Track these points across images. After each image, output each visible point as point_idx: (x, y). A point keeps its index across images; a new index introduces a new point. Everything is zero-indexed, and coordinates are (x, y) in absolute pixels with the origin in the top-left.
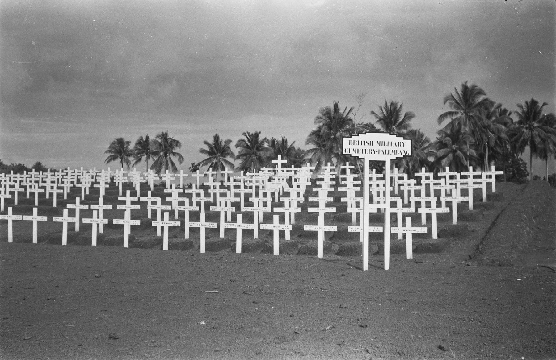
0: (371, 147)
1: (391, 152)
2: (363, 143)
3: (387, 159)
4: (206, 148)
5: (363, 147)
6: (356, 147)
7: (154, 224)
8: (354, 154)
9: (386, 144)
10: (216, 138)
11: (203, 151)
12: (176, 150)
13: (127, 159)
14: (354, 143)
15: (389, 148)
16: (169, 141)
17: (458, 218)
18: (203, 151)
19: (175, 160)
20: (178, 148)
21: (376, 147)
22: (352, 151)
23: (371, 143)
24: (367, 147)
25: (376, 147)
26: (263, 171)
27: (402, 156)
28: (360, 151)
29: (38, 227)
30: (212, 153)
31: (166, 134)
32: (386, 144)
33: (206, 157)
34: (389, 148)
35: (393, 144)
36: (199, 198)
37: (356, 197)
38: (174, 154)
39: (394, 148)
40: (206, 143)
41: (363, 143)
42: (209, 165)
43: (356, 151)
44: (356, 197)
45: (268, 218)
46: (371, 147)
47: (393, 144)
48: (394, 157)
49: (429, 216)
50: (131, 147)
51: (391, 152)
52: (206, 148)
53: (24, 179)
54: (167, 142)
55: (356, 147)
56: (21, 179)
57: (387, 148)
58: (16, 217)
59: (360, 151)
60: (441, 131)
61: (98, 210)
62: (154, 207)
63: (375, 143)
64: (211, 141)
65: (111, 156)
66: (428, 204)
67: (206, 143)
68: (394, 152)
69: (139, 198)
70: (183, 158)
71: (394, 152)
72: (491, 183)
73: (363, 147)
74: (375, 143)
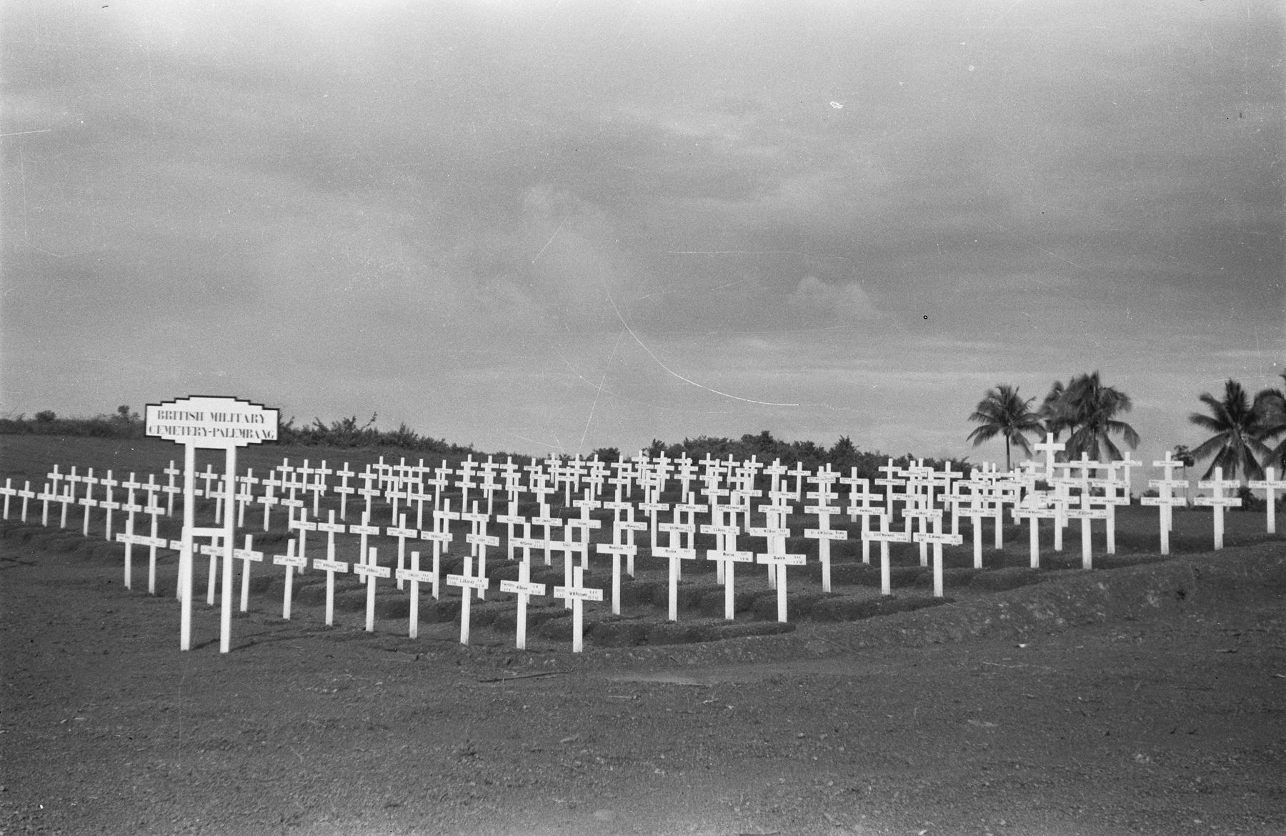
0: (199, 424)
1: (237, 433)
3: (230, 446)
4: (1208, 412)
5: (184, 423)
6: (170, 423)
8: (166, 436)
9: (228, 418)
10: (1233, 388)
11: (1199, 419)
12: (1118, 417)
13: (1019, 435)
14: (167, 416)
15: (235, 425)
16: (1102, 394)
17: (419, 620)
18: (1199, 419)
19: (1116, 438)
20: (1123, 411)
21: (208, 423)
22: (163, 430)
23: (198, 416)
24: (192, 423)
25: (208, 423)
26: (1023, 471)
27: (259, 441)
28: (179, 431)
29: (180, 617)
30: (1220, 424)
31: (1095, 377)
32: (228, 418)
33: (1207, 434)
34: (235, 425)
35: (242, 418)
36: (519, 540)
37: (788, 552)
39: (243, 425)
40: (1206, 399)
42: (1215, 453)
43: (171, 430)
44: (788, 552)
46: (199, 424)
47: (242, 418)
48: (243, 442)
50: (1034, 407)
51: (237, 433)
52: (1208, 412)
53: (946, 484)
54: (1097, 397)
55: (170, 423)
56: (937, 483)
57: (231, 426)
63: (207, 416)
64: (1220, 396)
65: (982, 428)
67: (1206, 399)
68: (244, 433)
69: (419, 533)
70: (1136, 435)
71: (244, 433)
72: (1103, 522)
73: (184, 423)
74: (207, 416)
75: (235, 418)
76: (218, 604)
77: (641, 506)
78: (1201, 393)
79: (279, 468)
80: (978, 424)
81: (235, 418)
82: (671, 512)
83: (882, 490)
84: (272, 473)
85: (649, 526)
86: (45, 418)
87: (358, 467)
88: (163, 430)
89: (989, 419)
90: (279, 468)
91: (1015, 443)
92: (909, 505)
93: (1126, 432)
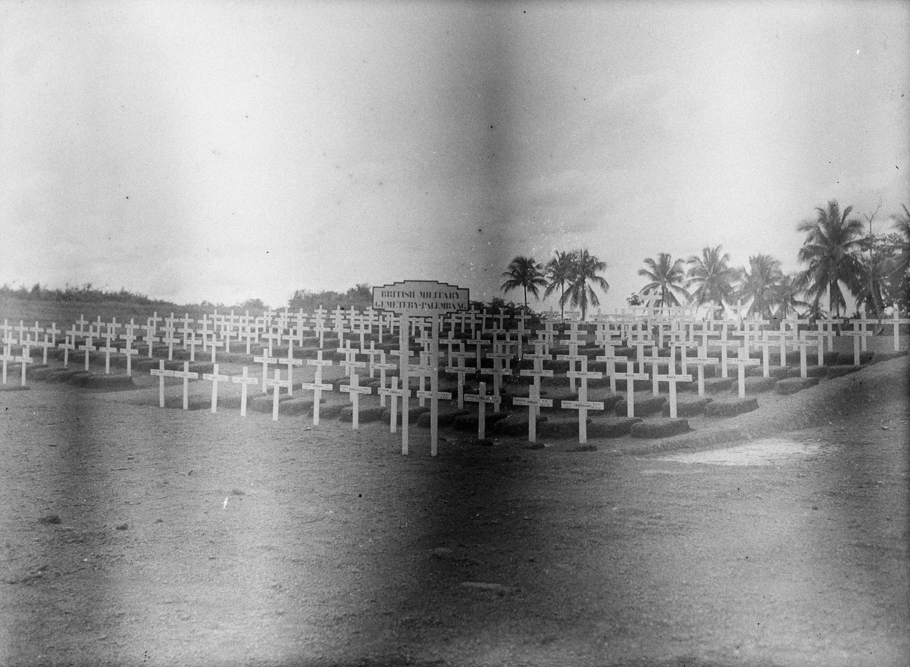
1: (439, 306)
2: (401, 295)
5: (401, 299)
6: (391, 299)
7: (87, 322)
11: (642, 272)
12: (598, 273)
18: (642, 272)
22: (385, 304)
33: (647, 281)
38: (595, 278)
40: (648, 261)
41: (401, 295)
45: (286, 332)
49: (225, 337)
51: (439, 306)
55: (391, 299)
58: (488, 316)
59: (397, 305)
60: (522, 259)
61: (499, 319)
62: (219, 323)
65: (511, 281)
66: (664, 370)
67: (648, 261)
75: (438, 295)
76: (399, 433)
77: (15, 342)
78: (644, 258)
79: (78, 322)
80: (509, 278)
81: (438, 295)
82: (57, 343)
83: (212, 319)
84: (74, 326)
85: (762, 362)
86: (124, 294)
87: (140, 322)
88: (385, 304)
89: (700, 280)
90: (78, 322)
91: (529, 290)
92: (673, 339)
93: (602, 284)
